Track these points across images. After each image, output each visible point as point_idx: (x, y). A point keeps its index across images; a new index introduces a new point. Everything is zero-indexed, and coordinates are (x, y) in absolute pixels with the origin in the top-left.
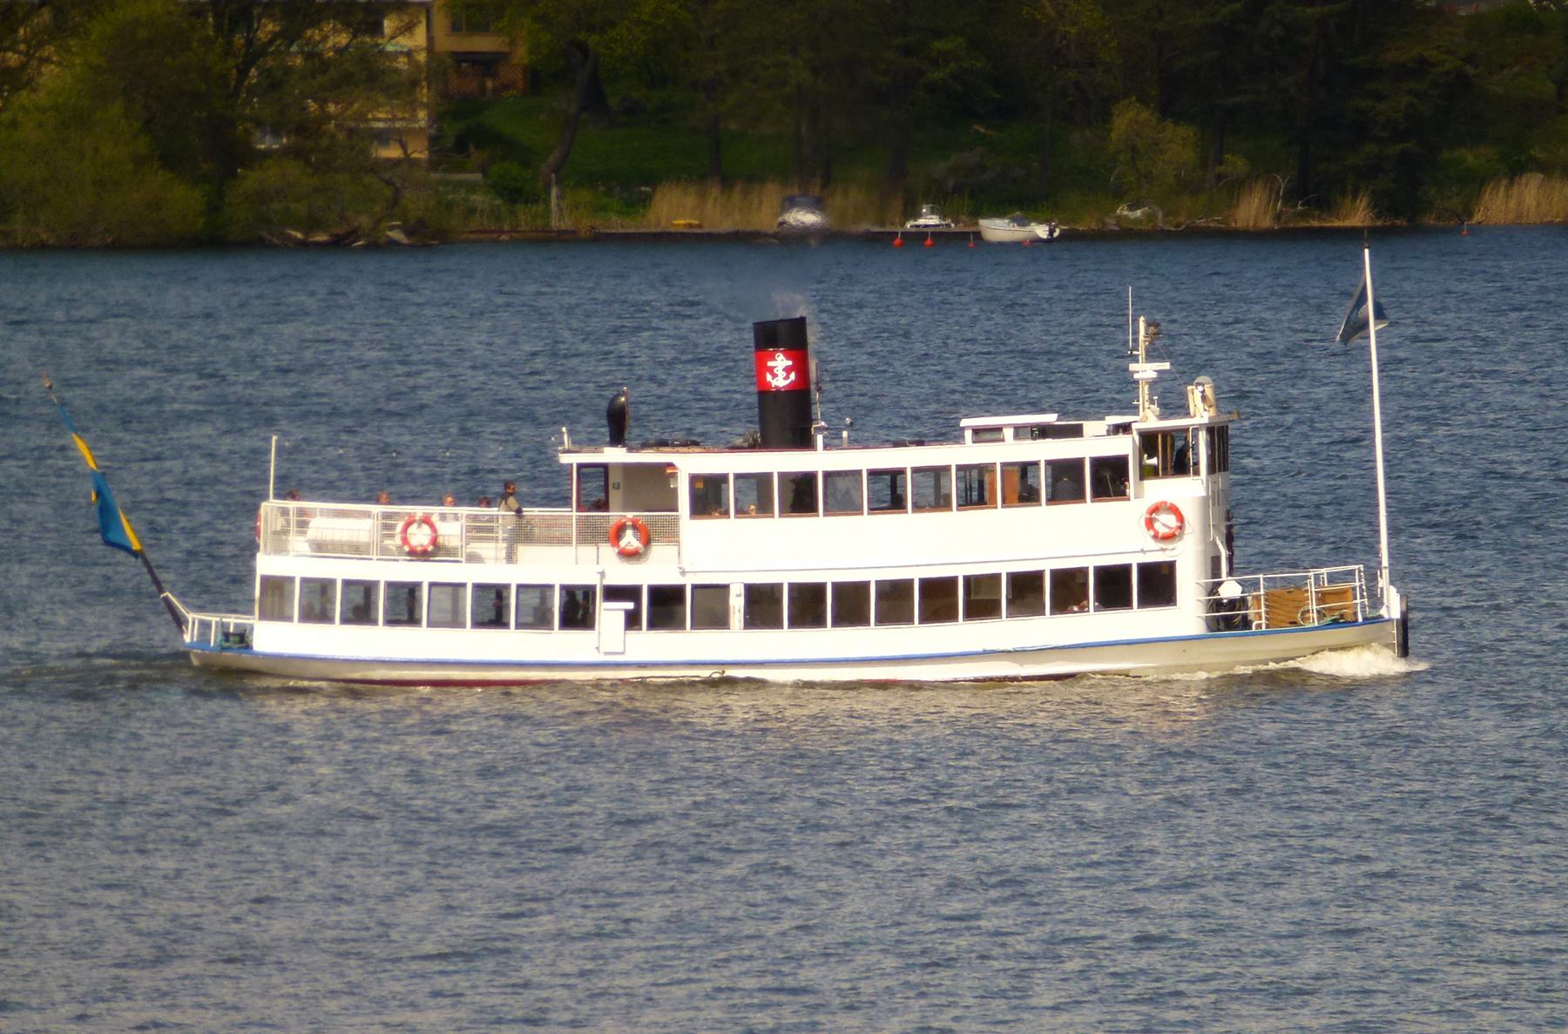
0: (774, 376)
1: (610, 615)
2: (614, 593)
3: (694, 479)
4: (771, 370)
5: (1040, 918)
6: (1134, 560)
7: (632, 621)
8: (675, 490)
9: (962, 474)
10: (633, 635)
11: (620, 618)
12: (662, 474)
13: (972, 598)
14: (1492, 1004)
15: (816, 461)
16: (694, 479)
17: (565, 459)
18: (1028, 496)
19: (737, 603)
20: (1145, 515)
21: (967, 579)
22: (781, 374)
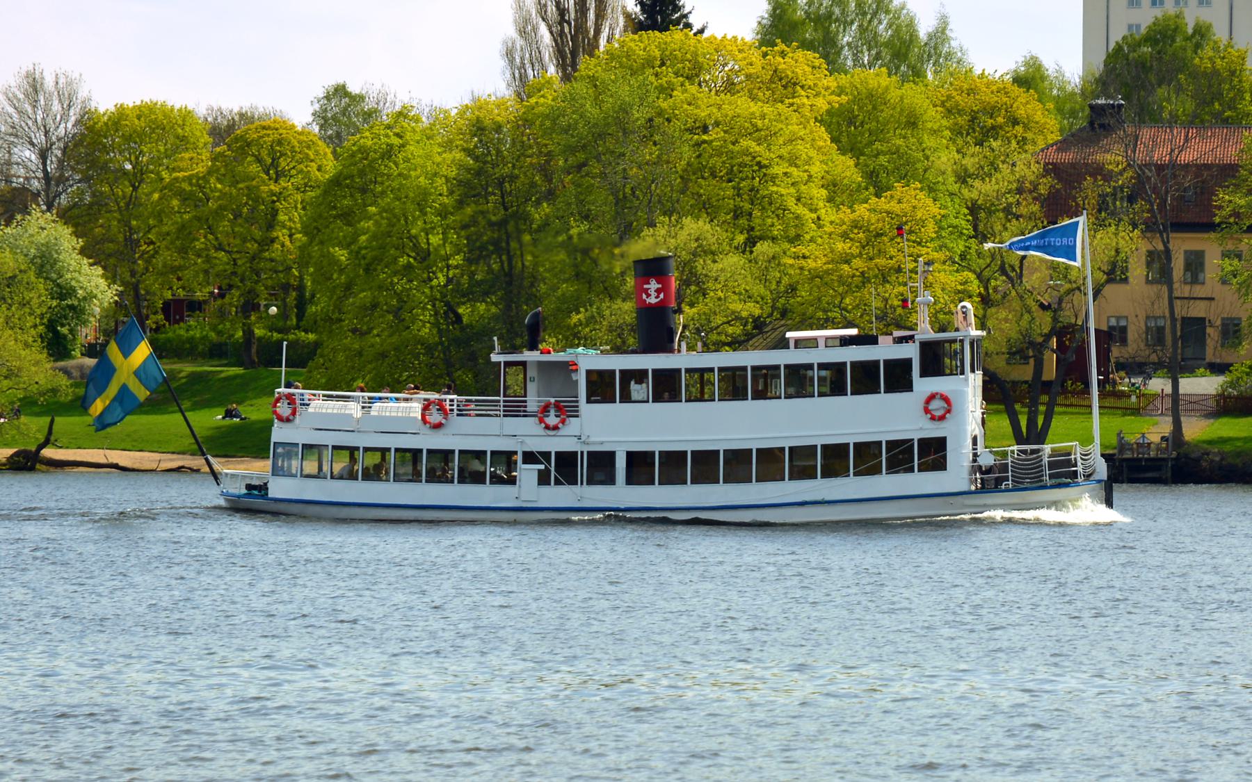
0: (649, 295)
1: (527, 474)
2: (530, 457)
3: (589, 372)
4: (646, 291)
5: (231, 763)
6: (916, 436)
7: (543, 479)
8: (521, 352)
9: (809, 389)
10: (545, 489)
11: (534, 477)
12: (568, 368)
13: (795, 463)
14: (963, 521)
15: (681, 359)
16: (589, 372)
17: (495, 358)
18: (837, 389)
19: (621, 463)
20: (937, 423)
21: (791, 448)
22: (653, 294)
